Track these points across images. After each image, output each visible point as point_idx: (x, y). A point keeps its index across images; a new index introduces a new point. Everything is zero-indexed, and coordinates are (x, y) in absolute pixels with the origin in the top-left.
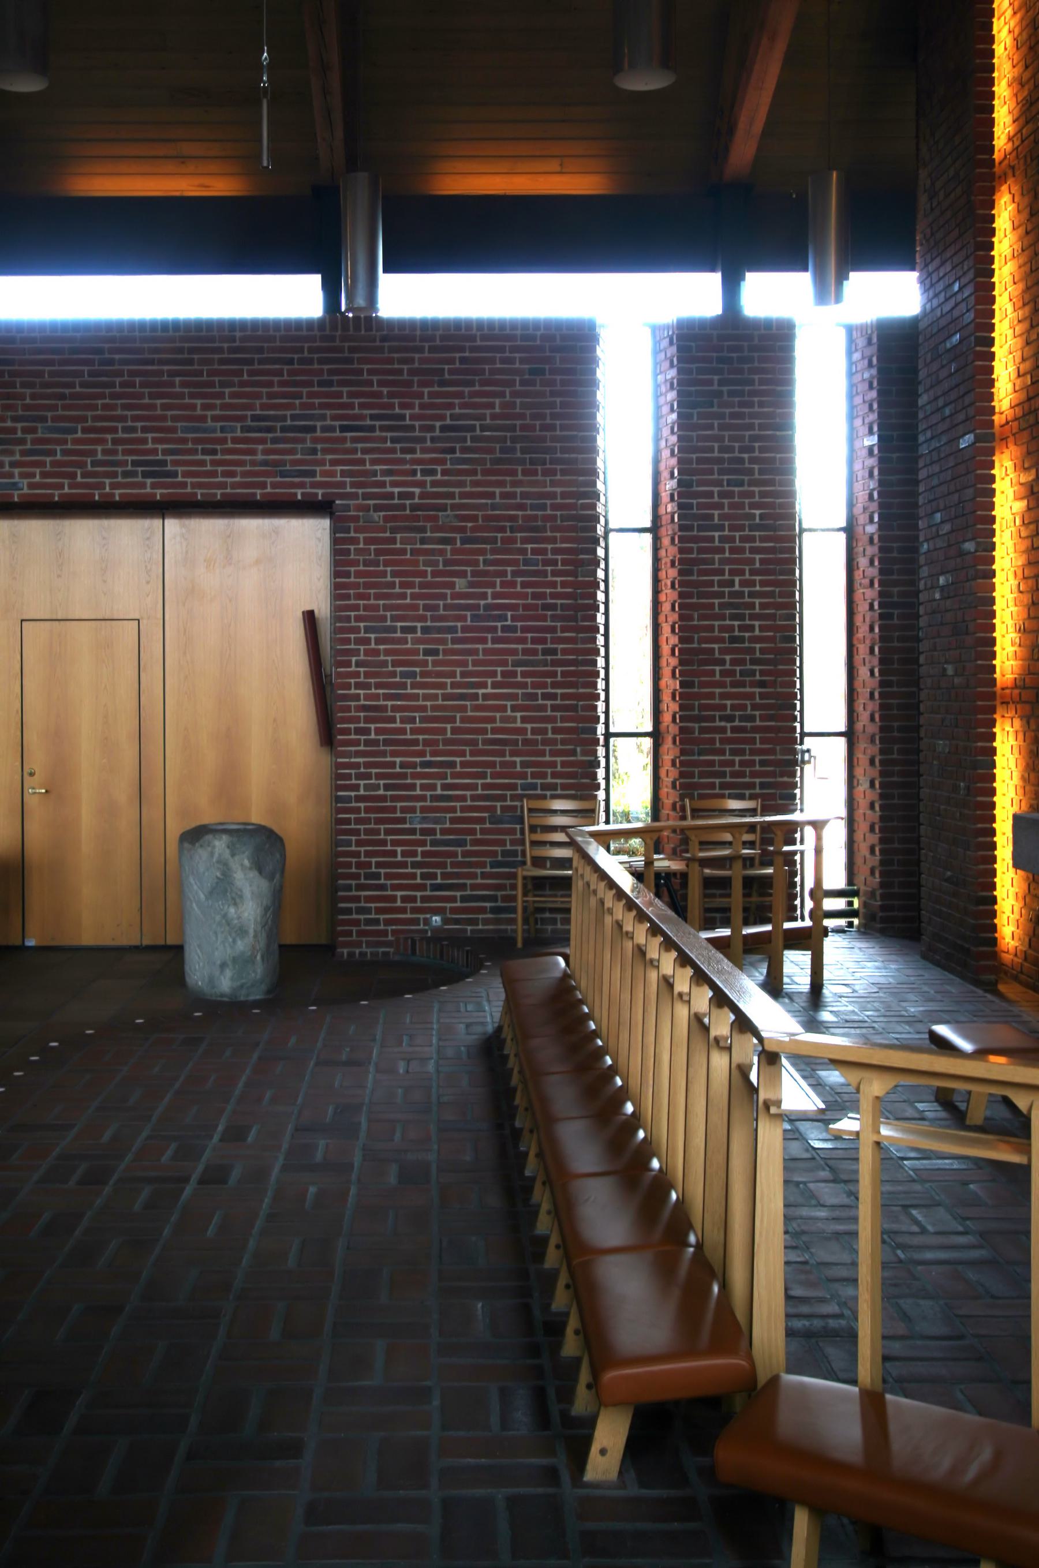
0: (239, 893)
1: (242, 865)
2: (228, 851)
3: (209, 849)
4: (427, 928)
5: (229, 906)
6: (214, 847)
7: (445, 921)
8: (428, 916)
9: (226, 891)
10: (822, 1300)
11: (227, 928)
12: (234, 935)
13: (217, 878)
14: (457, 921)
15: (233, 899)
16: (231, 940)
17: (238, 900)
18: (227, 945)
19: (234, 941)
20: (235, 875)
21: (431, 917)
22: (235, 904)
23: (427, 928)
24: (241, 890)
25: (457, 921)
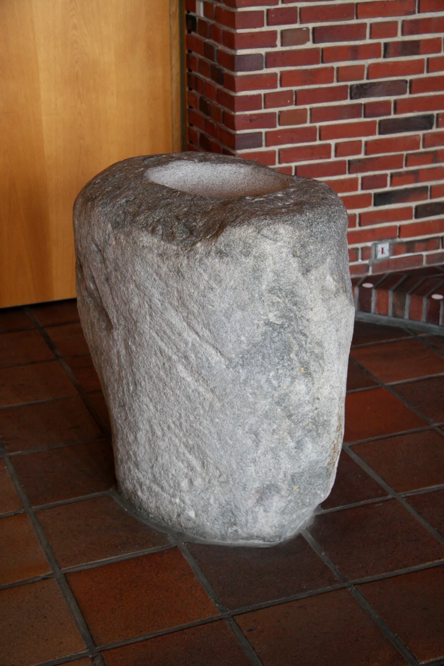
0: (317, 351)
1: (323, 289)
2: (294, 263)
3: (250, 262)
4: (367, 262)
5: (294, 378)
6: (261, 257)
7: (395, 250)
8: (369, 244)
9: (288, 348)
10: (118, 299)
11: (286, 423)
12: (299, 433)
13: (268, 323)
14: (410, 247)
15: (305, 365)
16: (292, 444)
17: (313, 366)
18: (282, 454)
19: (299, 445)
20: (310, 315)
21: (375, 245)
22: (308, 374)
23: (367, 262)
24: (319, 344)
25: (410, 247)
